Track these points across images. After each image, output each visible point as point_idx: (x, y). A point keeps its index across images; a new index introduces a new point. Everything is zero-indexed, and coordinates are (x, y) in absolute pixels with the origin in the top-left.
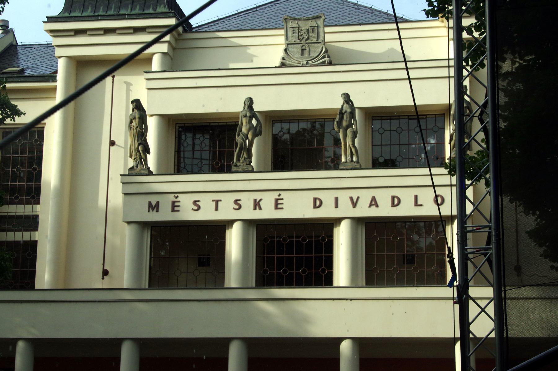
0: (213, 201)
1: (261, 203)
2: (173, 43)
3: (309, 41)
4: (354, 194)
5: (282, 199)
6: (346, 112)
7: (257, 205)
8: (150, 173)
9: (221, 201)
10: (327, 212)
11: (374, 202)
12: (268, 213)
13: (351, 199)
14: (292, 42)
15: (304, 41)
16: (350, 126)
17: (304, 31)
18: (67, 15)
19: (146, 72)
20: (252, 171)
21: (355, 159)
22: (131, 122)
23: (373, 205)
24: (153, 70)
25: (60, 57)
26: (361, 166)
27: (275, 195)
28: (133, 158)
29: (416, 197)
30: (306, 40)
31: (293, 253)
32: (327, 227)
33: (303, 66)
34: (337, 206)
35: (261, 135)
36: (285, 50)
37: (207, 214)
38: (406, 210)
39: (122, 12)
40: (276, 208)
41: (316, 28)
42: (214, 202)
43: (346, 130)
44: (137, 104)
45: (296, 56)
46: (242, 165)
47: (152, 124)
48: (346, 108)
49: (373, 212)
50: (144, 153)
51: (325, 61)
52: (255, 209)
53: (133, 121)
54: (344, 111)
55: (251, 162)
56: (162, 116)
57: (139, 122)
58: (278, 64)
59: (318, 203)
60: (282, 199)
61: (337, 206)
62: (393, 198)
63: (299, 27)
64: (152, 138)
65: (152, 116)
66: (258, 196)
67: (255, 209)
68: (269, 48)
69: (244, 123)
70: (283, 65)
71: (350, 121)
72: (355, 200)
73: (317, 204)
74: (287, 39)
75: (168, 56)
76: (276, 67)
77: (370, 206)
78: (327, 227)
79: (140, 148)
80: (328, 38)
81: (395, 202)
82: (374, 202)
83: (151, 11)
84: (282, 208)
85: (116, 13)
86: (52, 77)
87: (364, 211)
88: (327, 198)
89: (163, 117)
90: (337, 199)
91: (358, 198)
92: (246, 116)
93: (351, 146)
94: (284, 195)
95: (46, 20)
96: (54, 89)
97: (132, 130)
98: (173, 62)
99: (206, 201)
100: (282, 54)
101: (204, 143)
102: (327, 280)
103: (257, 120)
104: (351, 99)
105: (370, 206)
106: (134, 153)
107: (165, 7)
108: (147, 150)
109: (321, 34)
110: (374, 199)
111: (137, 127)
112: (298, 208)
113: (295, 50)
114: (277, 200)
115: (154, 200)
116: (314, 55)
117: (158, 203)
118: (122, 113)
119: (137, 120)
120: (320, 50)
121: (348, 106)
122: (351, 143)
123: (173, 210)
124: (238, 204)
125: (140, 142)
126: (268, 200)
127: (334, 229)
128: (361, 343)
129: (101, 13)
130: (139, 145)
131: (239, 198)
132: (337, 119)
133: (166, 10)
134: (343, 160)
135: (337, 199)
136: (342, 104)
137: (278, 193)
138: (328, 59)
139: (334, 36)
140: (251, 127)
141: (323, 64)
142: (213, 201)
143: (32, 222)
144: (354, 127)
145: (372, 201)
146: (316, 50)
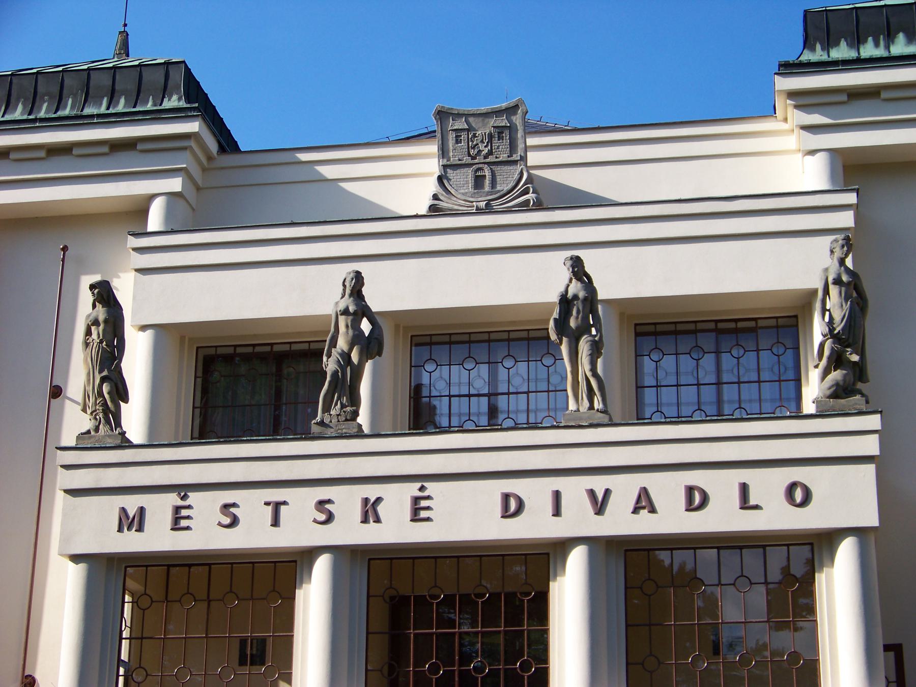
0: (267, 504)
1: (380, 509)
3: (491, 159)
4: (599, 483)
5: (428, 498)
6: (575, 297)
7: (370, 512)
8: (125, 443)
9: (285, 503)
10: (536, 525)
11: (644, 502)
12: (395, 529)
13: (592, 493)
14: (454, 160)
15: (479, 159)
16: (584, 329)
17: (480, 138)
19: (134, 235)
20: (359, 434)
21: (598, 405)
23: (644, 508)
24: (150, 229)
26: (611, 419)
27: (413, 489)
28: (89, 411)
29: (744, 489)
30: (485, 157)
33: (479, 212)
34: (557, 512)
35: (380, 355)
36: (440, 179)
37: (254, 534)
38: (722, 517)
40: (416, 517)
41: (507, 132)
42: (270, 508)
43: (577, 340)
44: (104, 293)
45: (462, 191)
46: (334, 420)
48: (576, 288)
50: (112, 401)
51: (528, 200)
52: (365, 520)
53: (93, 328)
54: (570, 295)
55: (356, 414)
56: (160, 329)
57: (104, 330)
58: (423, 211)
59: (513, 505)
60: (428, 498)
61: (557, 512)
62: (690, 490)
63: (468, 130)
66: (372, 491)
67: (365, 520)
68: (407, 181)
69: (342, 328)
70: (435, 210)
72: (600, 497)
73: (512, 507)
74: (443, 152)
75: (181, 202)
76: (417, 216)
77: (636, 511)
79: (106, 388)
81: (696, 500)
82: (644, 502)
83: (149, 106)
84: (428, 519)
85: (74, 113)
87: (621, 522)
89: (162, 331)
90: (557, 495)
91: (607, 492)
92: (346, 312)
93: (589, 374)
94: (432, 488)
97: (89, 350)
98: (191, 214)
100: (432, 186)
101: (249, 385)
103: (372, 321)
104: (588, 269)
105: (636, 511)
106: (92, 400)
107: (179, 99)
108: (121, 392)
109: (521, 146)
110: (644, 493)
111: (101, 342)
112: (466, 517)
113: (462, 179)
114: (416, 500)
115: (132, 503)
116: (503, 187)
117: (142, 510)
119: (101, 328)
120: (516, 176)
121: (579, 284)
122: (587, 367)
124: (326, 513)
125: (105, 373)
127: (551, 583)
130: (103, 380)
131: (326, 498)
132: (556, 315)
133: (183, 104)
134: (572, 406)
135: (557, 495)
136: (567, 281)
137: (419, 485)
138: (534, 195)
140: (357, 338)
141: (525, 207)
142: (267, 504)
144: (594, 332)
145: (639, 496)
146: (507, 178)
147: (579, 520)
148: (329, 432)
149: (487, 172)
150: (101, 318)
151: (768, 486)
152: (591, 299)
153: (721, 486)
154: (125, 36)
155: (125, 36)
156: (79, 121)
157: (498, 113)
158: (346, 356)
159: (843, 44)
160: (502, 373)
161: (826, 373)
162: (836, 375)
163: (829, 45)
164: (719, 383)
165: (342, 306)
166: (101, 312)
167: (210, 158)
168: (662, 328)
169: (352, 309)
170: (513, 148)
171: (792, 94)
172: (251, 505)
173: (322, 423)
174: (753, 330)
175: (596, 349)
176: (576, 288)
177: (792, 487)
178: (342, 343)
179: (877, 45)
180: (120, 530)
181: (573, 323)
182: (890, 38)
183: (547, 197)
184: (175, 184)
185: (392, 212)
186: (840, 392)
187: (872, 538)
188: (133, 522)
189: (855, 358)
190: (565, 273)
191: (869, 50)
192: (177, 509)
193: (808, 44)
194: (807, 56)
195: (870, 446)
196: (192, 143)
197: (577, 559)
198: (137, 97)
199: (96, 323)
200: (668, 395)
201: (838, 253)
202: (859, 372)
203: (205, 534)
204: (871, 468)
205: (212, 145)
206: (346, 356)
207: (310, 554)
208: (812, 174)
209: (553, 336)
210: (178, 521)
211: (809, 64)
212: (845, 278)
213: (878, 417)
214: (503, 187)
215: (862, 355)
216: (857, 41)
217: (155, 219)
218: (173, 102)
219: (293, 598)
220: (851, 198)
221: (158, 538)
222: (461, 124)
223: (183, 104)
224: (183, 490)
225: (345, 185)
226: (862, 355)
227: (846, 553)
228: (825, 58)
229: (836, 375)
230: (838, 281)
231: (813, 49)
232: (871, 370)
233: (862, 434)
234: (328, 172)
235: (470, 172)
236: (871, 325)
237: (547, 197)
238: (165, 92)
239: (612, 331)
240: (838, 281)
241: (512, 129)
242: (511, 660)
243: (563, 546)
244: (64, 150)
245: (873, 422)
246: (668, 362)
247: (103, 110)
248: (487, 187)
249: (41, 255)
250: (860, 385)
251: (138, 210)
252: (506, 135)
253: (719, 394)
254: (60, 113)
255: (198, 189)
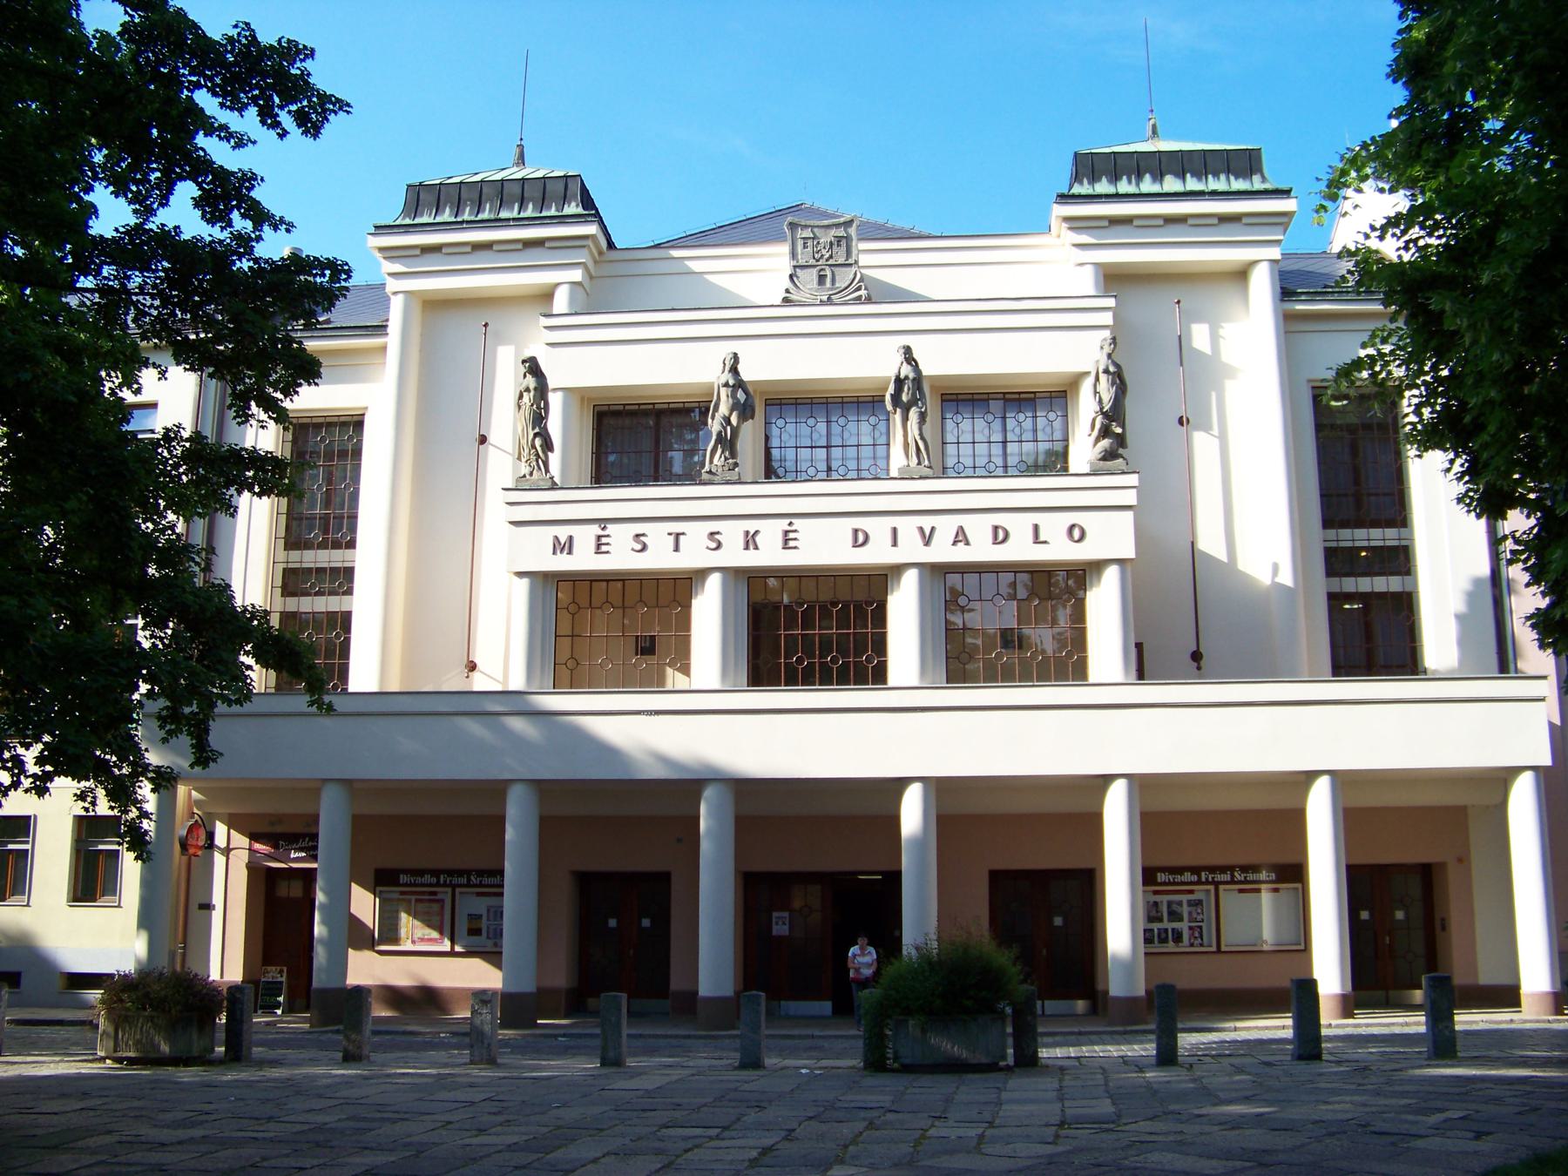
1: (758, 539)
2: (591, 265)
4: (927, 522)
6: (907, 377)
7: (750, 541)
10: (877, 554)
11: (961, 537)
12: (770, 555)
13: (921, 529)
14: (802, 262)
18: (408, 221)
22: (521, 396)
25: (395, 293)
27: (783, 524)
29: (1036, 528)
31: (810, 632)
32: (879, 580)
33: (822, 303)
34: (895, 544)
36: (791, 277)
37: (660, 558)
38: (1021, 550)
39: (504, 214)
40: (786, 545)
43: (908, 410)
44: (533, 367)
47: (555, 400)
48: (906, 371)
49: (961, 555)
52: (747, 548)
59: (861, 538)
61: (895, 544)
62: (996, 528)
64: (554, 425)
65: (555, 390)
66: (752, 526)
67: (747, 548)
70: (786, 300)
71: (914, 394)
73: (860, 539)
74: (794, 255)
77: (955, 543)
78: (879, 580)
79: (538, 442)
80: (864, 260)
81: (1000, 536)
82: (961, 537)
83: (553, 212)
85: (492, 217)
86: (381, 329)
87: (944, 552)
88: (1019, 526)
90: (895, 530)
92: (726, 385)
94: (798, 523)
95: (372, 230)
96: (384, 348)
98: (591, 299)
99: (585, 537)
101: (638, 438)
102: (878, 676)
103: (746, 392)
105: (955, 543)
108: (548, 446)
109: (854, 252)
110: (961, 530)
112: (825, 547)
114: (786, 532)
115: (563, 532)
116: (840, 284)
118: (507, 380)
122: (916, 433)
123: (786, 547)
126: (771, 532)
128: (942, 790)
129: (466, 216)
130: (536, 435)
133: (580, 210)
135: (895, 530)
139: (873, 260)
143: (343, 579)
147: (911, 550)
148: (716, 479)
149: (828, 272)
150: (532, 386)
151: (1054, 526)
152: (918, 380)
153: (1019, 526)
154: (521, 147)
155: (521, 147)
156: (497, 223)
157: (837, 226)
158: (727, 420)
159: (1104, 179)
160: (835, 429)
161: (1097, 440)
162: (1105, 443)
163: (1094, 179)
164: (1005, 442)
165: (723, 380)
166: (531, 382)
167: (601, 253)
168: (965, 398)
169: (731, 382)
170: (848, 254)
171: (1067, 219)
172: (657, 535)
173: (710, 472)
174: (1033, 400)
175: (922, 417)
176: (906, 371)
177: (1072, 527)
178: (724, 409)
179: (1130, 182)
180: (554, 553)
181: (905, 398)
182: (1140, 177)
183: (874, 293)
184: (577, 275)
185: (738, 296)
186: (1109, 455)
187: (1129, 567)
188: (567, 547)
189: (1119, 430)
190: (900, 357)
191: (1124, 187)
192: (599, 537)
193: (1077, 178)
194: (1077, 190)
195: (1130, 498)
196: (590, 243)
197: (910, 579)
198: (542, 203)
199: (528, 390)
200: (966, 450)
201: (1107, 349)
202: (1121, 440)
203: (621, 557)
204: (1129, 515)
205: (604, 244)
206: (727, 420)
207: (703, 573)
208: (1086, 282)
209: (889, 407)
210: (600, 546)
211: (1080, 196)
212: (1112, 369)
213: (1136, 476)
214: (840, 284)
215: (1123, 427)
216: (1114, 179)
217: (561, 302)
218: (573, 208)
219: (689, 606)
220: (1111, 302)
221: (584, 560)
222: (807, 233)
223: (580, 210)
224: (603, 522)
225: (709, 277)
226: (1123, 427)
227: (1111, 575)
228: (1090, 192)
229: (1105, 443)
230: (1106, 371)
231: (1081, 183)
232: (1129, 439)
233: (1124, 488)
234: (695, 266)
235: (815, 271)
236: (1129, 403)
237: (874, 293)
238: (565, 199)
239: (932, 404)
240: (1106, 371)
241: (848, 238)
242: (858, 654)
243: (898, 569)
244: (538, 243)
245: (1133, 480)
246: (966, 425)
247: (515, 214)
248: (828, 284)
249: (466, 327)
250: (1121, 451)
251: (547, 295)
252: (843, 243)
253: (1005, 448)
254: (480, 217)
255: (591, 277)
